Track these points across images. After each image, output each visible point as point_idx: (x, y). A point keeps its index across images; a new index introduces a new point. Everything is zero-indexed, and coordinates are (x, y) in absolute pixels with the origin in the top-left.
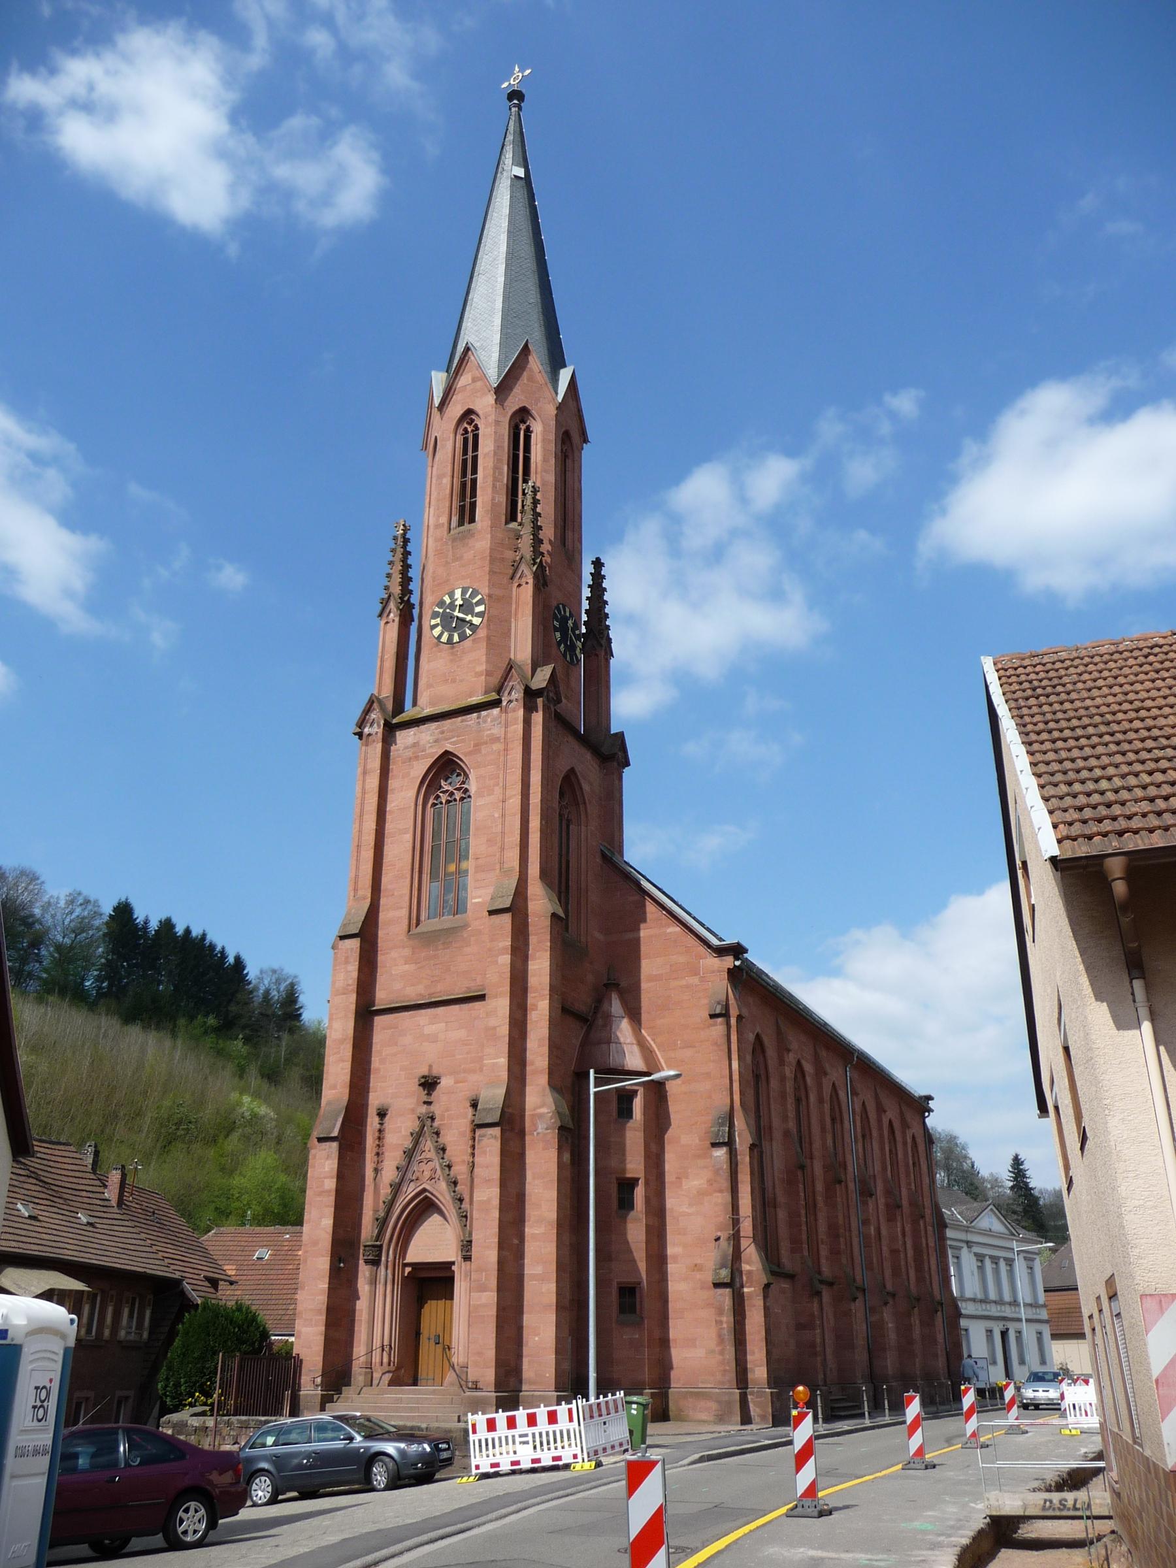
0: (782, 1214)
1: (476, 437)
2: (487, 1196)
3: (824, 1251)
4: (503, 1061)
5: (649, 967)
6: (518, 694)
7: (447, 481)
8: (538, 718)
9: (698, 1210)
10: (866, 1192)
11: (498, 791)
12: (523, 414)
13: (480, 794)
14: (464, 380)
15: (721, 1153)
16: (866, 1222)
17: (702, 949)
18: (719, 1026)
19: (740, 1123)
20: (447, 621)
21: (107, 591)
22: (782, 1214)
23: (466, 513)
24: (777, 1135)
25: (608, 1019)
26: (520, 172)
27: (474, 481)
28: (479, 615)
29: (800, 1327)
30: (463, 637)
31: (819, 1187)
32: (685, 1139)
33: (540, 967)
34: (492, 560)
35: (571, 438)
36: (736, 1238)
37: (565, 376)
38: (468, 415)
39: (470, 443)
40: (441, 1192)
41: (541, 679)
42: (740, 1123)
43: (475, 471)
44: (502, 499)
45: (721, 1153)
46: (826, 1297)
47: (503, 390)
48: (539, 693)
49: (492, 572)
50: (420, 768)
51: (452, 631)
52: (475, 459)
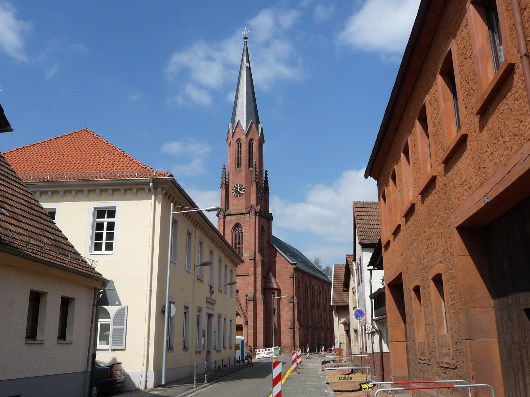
0: (302, 314)
1: (241, 145)
2: (250, 313)
3: (310, 321)
4: (253, 289)
5: (278, 266)
6: (253, 213)
7: (234, 156)
8: (257, 218)
9: (287, 315)
10: (319, 307)
11: (249, 232)
12: (251, 140)
13: (245, 233)
14: (238, 130)
15: (291, 304)
16: (319, 314)
17: (288, 263)
18: (291, 280)
19: (295, 298)
20: (236, 191)
21: (32, 44)
22: (302, 314)
23: (239, 164)
24: (302, 299)
25: (270, 278)
26: (248, 65)
27: (241, 156)
28: (244, 191)
29: (305, 335)
30: (240, 196)
31: (309, 307)
32: (284, 301)
33: (259, 270)
34: (246, 178)
35: (262, 141)
36: (294, 320)
37: (260, 126)
38: (239, 139)
39: (239, 146)
40: (240, 312)
41: (258, 209)
42: (295, 298)
43: (241, 154)
44: (248, 163)
45: (291, 304)
46: (310, 329)
47: (247, 135)
48: (258, 212)
49: (246, 181)
50: (232, 225)
51: (237, 194)
52: (241, 150)
